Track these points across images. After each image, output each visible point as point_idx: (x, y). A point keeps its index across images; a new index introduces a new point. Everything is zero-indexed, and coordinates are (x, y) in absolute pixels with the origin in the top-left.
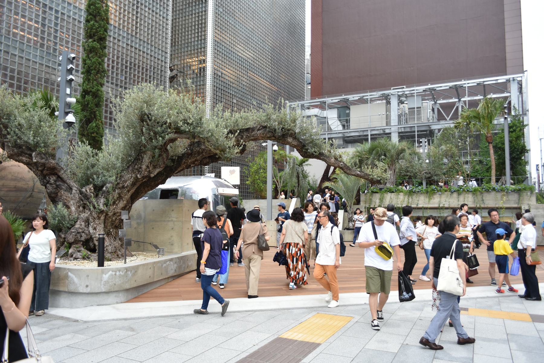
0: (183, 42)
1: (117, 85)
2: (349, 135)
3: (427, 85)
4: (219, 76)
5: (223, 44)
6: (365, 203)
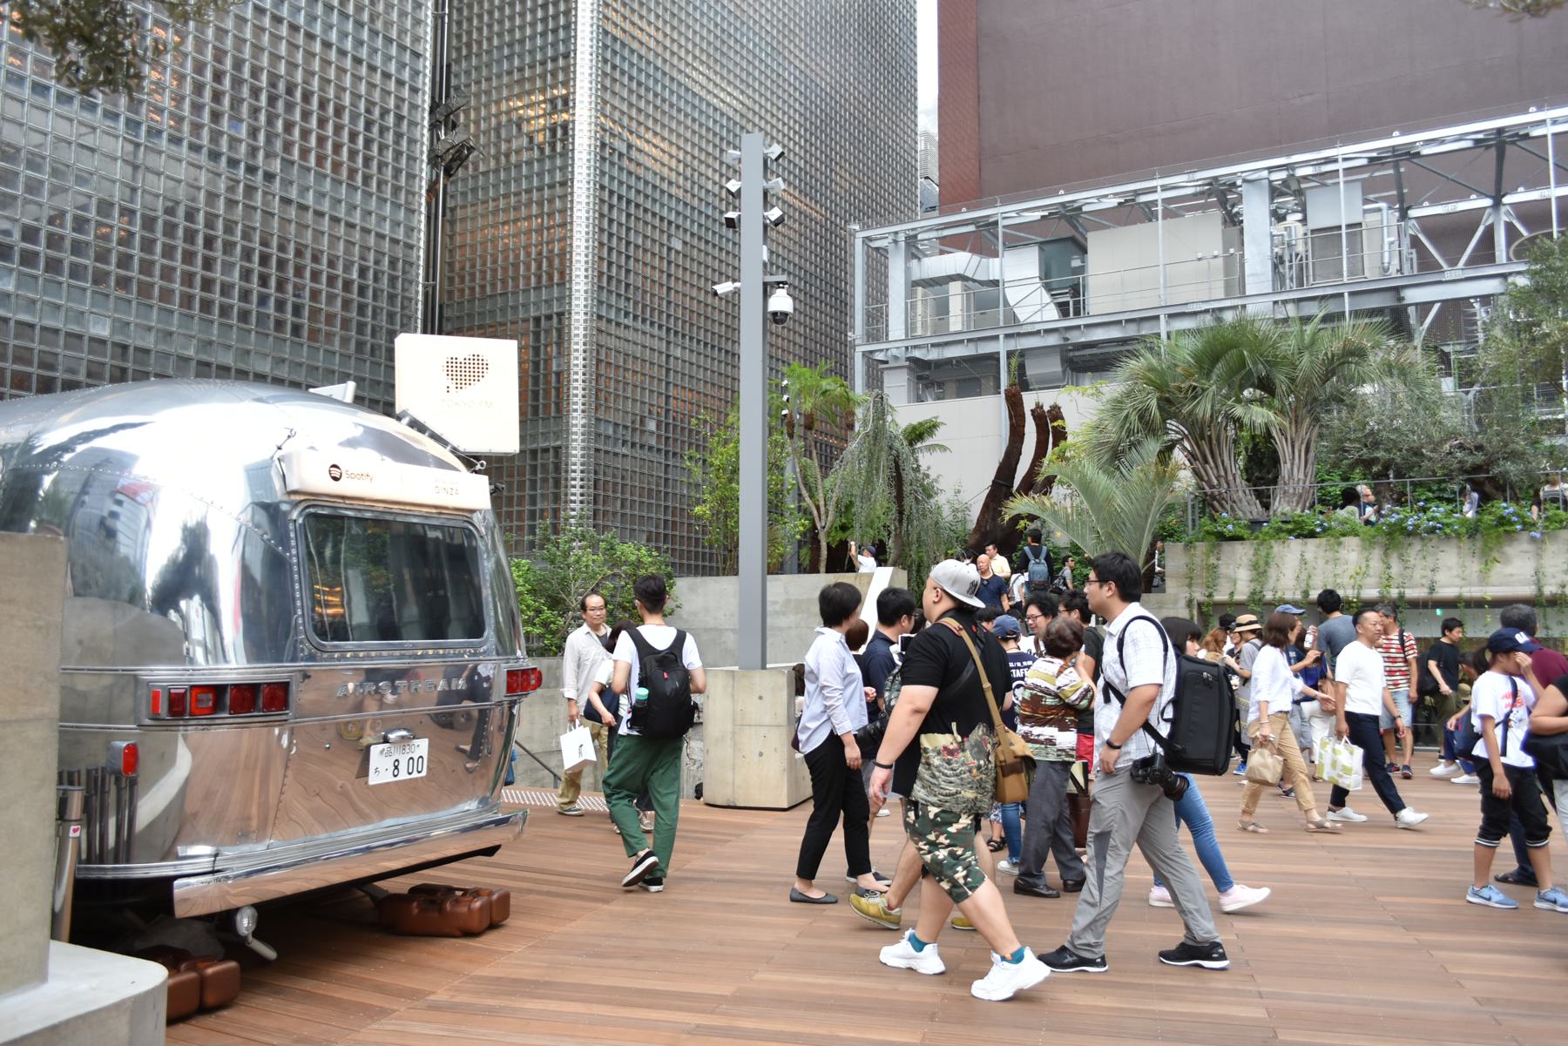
0: (495, 42)
1: (215, 156)
2: (1083, 340)
3: (1389, 135)
4: (621, 155)
5: (635, 45)
6: (1190, 586)
